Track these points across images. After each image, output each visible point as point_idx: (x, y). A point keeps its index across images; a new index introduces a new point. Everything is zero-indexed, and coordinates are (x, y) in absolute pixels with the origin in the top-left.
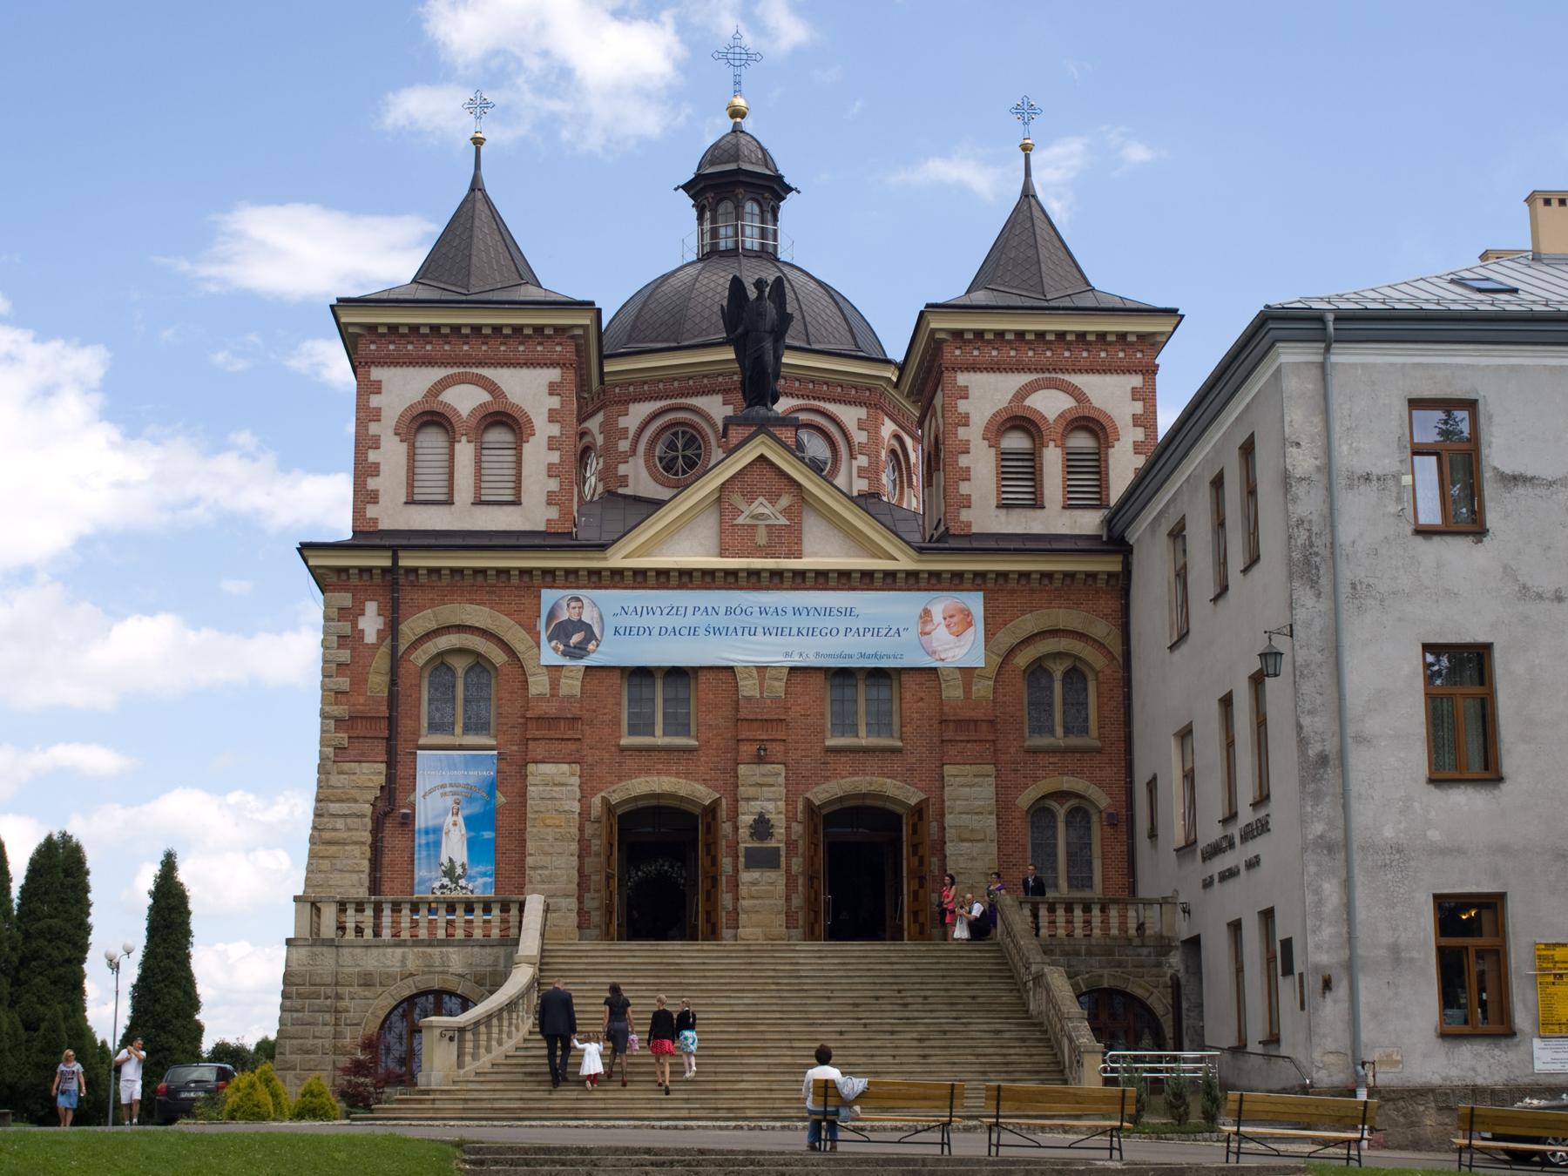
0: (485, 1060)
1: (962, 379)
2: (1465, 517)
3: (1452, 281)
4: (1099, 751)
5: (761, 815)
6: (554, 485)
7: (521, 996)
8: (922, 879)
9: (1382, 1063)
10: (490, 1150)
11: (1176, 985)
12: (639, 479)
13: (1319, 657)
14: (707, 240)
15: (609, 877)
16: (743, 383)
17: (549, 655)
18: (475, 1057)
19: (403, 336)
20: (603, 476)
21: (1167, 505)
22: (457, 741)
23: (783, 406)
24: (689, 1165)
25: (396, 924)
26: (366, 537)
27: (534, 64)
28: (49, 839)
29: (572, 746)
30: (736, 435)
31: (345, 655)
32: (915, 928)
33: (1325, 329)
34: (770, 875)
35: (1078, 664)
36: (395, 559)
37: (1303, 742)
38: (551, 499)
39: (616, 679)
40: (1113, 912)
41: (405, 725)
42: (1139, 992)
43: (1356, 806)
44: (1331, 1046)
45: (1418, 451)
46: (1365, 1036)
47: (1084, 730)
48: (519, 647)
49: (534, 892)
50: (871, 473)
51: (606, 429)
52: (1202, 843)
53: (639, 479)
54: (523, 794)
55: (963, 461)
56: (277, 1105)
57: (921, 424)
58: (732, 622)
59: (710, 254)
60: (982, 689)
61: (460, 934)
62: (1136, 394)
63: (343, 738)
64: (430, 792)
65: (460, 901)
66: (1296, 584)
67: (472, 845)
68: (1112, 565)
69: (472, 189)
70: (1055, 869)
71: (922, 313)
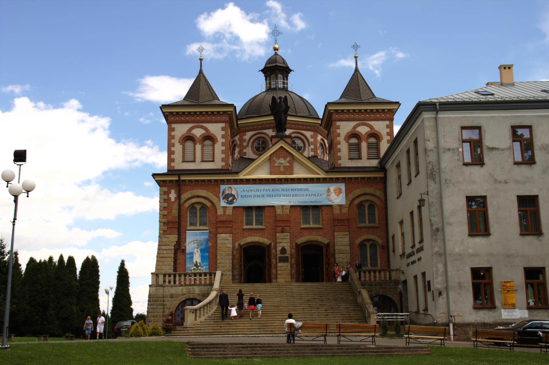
0: (203, 318)
1: (338, 123)
2: (478, 160)
3: (475, 92)
4: (379, 227)
6: (223, 156)
7: (213, 300)
8: (329, 265)
9: (457, 316)
10: (196, 345)
11: (401, 294)
12: (249, 153)
13: (436, 201)
14: (268, 85)
15: (241, 266)
16: (276, 126)
17: (223, 203)
18: (200, 317)
19: (180, 115)
20: (239, 153)
21: (395, 158)
22: (197, 228)
23: (288, 132)
24: (252, 347)
25: (180, 280)
26: (171, 171)
27: (228, 36)
28: (88, 258)
29: (230, 229)
30: (274, 140)
31: (166, 205)
33: (436, 107)
34: (286, 264)
36: (179, 177)
37: (432, 225)
38: (223, 160)
39: (242, 210)
40: (382, 273)
41: (183, 224)
42: (390, 296)
43: (447, 243)
44: (442, 311)
45: (464, 141)
46: (452, 307)
47: (374, 222)
48: (214, 201)
49: (220, 270)
50: (315, 150)
51: (239, 139)
52: (406, 254)
53: (249, 153)
54: (216, 243)
55: (339, 146)
56: (144, 332)
57: (328, 136)
58: (274, 193)
59: (269, 89)
60: (345, 210)
61: (198, 282)
62: (388, 127)
63: (165, 228)
65: (198, 273)
66: (429, 180)
67: (202, 257)
68: (381, 175)
69: (200, 73)
70: (367, 261)
71: (326, 105)
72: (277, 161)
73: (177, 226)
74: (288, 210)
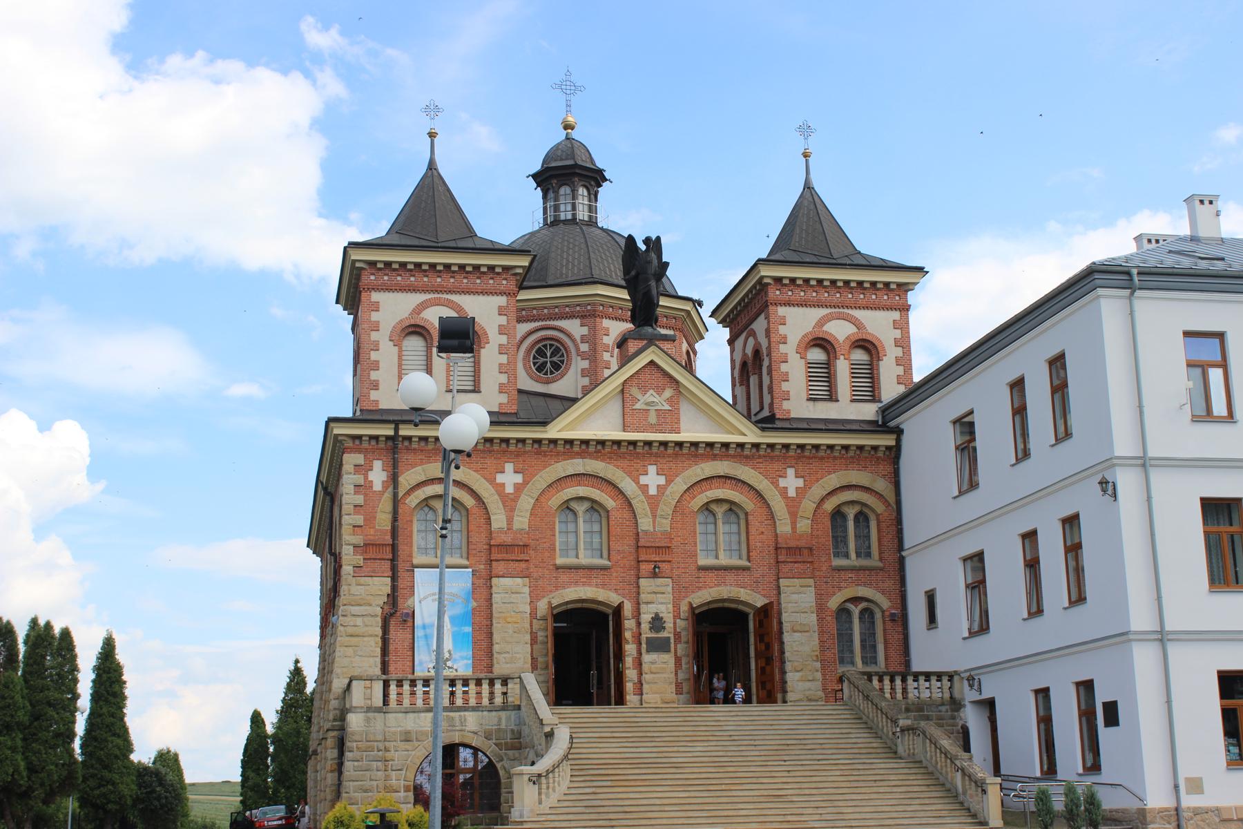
4: (881, 569)
5: (657, 614)
26: (366, 415)
29: (523, 565)
32: (763, 694)
33: (1131, 280)
35: (866, 510)
36: (396, 430)
47: (869, 555)
59: (553, 223)
61: (472, 702)
64: (425, 598)
68: (889, 441)
72: (639, 396)
73: (390, 556)
74: (668, 522)
